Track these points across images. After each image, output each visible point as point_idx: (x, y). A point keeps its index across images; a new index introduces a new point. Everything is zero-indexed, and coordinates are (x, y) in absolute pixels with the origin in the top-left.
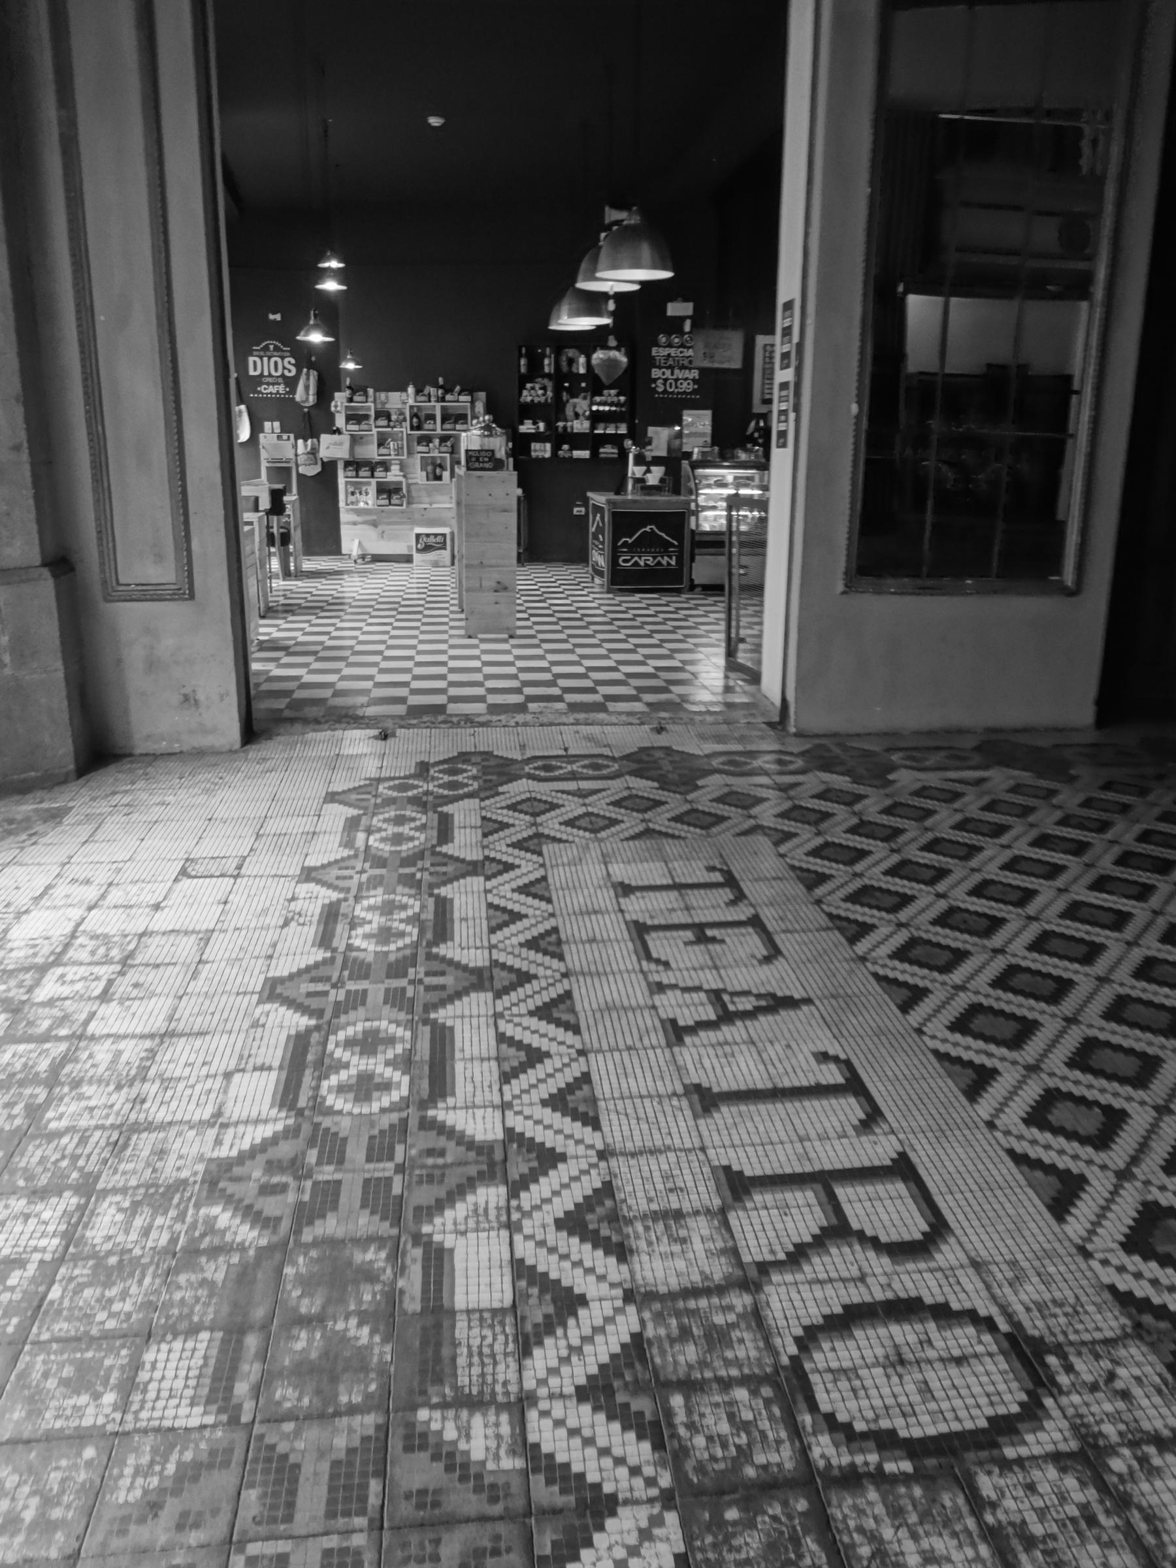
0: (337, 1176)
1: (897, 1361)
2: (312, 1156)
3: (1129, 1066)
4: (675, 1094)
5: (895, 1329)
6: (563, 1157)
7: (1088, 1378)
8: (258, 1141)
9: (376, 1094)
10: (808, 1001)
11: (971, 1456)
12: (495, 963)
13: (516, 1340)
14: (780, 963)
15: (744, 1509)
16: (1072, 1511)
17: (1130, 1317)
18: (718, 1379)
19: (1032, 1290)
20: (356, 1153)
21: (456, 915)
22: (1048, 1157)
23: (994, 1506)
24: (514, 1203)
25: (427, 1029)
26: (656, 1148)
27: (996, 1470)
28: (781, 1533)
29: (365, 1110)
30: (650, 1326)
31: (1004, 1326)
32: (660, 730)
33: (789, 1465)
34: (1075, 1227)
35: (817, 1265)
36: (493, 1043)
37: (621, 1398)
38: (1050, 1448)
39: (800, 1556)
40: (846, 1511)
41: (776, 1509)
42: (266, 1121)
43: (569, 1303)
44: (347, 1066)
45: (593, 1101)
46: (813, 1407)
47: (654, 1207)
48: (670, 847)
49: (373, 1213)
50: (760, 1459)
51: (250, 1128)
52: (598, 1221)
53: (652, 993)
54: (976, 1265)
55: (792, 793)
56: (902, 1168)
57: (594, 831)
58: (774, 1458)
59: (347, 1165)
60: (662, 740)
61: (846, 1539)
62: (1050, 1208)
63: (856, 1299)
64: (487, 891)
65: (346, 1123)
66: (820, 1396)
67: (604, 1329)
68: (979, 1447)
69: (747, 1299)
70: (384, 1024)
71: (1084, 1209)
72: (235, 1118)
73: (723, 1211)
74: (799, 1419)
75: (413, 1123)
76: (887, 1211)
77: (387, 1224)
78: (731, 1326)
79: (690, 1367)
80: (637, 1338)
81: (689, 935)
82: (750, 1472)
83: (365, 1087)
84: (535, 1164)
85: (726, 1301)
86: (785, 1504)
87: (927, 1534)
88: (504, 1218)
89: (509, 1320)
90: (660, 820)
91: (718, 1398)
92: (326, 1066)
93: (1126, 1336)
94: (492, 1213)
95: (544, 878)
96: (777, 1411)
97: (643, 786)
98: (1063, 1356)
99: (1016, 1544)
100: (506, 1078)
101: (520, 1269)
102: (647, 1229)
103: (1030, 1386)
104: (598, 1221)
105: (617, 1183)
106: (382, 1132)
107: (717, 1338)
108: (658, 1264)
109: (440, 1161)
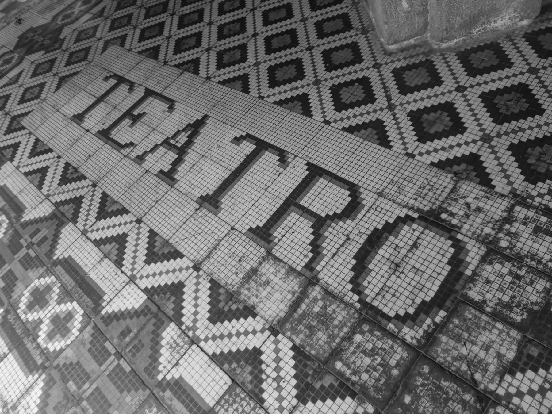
0: (94, 386)
1: (396, 267)
2: (72, 386)
3: (347, 55)
4: (197, 210)
5: (381, 252)
6: (82, 197)
7: (461, 213)
8: (38, 401)
9: (69, 325)
10: (206, 117)
11: (458, 287)
12: (57, 205)
13: (251, 398)
14: (177, 106)
15: (410, 392)
16: (509, 279)
17: (450, 172)
18: (343, 339)
19: (410, 190)
20: (91, 365)
21: (15, 192)
22: (231, 76)
23: (484, 302)
24: (183, 327)
25: (59, 267)
26: (212, 245)
27: (471, 285)
28: (431, 389)
29: (72, 338)
30: (294, 337)
31: (416, 215)
32: (19, 21)
33: (405, 355)
34: (253, 92)
35: (328, 247)
36: (25, 179)
37: (317, 386)
38: (478, 257)
39: (447, 393)
40: (442, 355)
41: (420, 381)
42: (31, 387)
43: (253, 356)
44: (40, 322)
45: (166, 243)
46: (389, 319)
47: (241, 275)
48: (78, 80)
49: (129, 391)
50: (393, 362)
51: (28, 398)
52: (227, 305)
53: (140, 165)
54: (380, 194)
55: (105, 14)
56: (315, 172)
57: (37, 97)
58: (397, 357)
59: (94, 376)
60: (24, 27)
61: (453, 368)
62: (242, 91)
63: (355, 250)
64: (18, 168)
65: (70, 353)
66: (386, 310)
67: (279, 358)
68: (457, 280)
69: (318, 288)
70: (36, 283)
71: (253, 84)
72: (15, 400)
73: (269, 253)
74: (388, 328)
75: (101, 325)
76: (326, 198)
77: (140, 391)
78: (325, 307)
79: (328, 343)
80: (294, 348)
81: (127, 121)
82: (395, 372)
83: (60, 325)
84: (173, 299)
85: (311, 297)
86: (420, 374)
87: (477, 337)
88: (187, 339)
89: (238, 390)
90: (62, 69)
91: (352, 349)
92: (31, 330)
93: (457, 182)
94: (179, 341)
95: (37, 140)
96: (378, 333)
97: (38, 57)
98: (446, 211)
99: (506, 312)
100: (119, 263)
101: (218, 359)
102: (248, 289)
103: (447, 235)
104: (227, 305)
105: (215, 277)
106: (91, 343)
107: (324, 319)
108: (269, 304)
109: (132, 335)
